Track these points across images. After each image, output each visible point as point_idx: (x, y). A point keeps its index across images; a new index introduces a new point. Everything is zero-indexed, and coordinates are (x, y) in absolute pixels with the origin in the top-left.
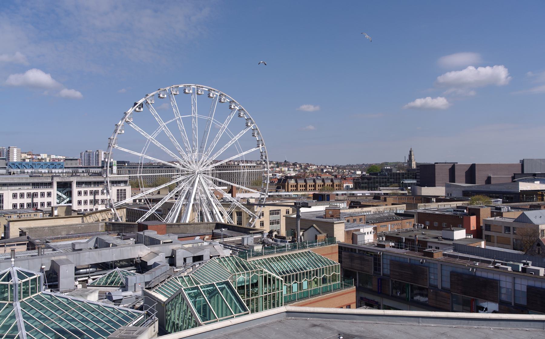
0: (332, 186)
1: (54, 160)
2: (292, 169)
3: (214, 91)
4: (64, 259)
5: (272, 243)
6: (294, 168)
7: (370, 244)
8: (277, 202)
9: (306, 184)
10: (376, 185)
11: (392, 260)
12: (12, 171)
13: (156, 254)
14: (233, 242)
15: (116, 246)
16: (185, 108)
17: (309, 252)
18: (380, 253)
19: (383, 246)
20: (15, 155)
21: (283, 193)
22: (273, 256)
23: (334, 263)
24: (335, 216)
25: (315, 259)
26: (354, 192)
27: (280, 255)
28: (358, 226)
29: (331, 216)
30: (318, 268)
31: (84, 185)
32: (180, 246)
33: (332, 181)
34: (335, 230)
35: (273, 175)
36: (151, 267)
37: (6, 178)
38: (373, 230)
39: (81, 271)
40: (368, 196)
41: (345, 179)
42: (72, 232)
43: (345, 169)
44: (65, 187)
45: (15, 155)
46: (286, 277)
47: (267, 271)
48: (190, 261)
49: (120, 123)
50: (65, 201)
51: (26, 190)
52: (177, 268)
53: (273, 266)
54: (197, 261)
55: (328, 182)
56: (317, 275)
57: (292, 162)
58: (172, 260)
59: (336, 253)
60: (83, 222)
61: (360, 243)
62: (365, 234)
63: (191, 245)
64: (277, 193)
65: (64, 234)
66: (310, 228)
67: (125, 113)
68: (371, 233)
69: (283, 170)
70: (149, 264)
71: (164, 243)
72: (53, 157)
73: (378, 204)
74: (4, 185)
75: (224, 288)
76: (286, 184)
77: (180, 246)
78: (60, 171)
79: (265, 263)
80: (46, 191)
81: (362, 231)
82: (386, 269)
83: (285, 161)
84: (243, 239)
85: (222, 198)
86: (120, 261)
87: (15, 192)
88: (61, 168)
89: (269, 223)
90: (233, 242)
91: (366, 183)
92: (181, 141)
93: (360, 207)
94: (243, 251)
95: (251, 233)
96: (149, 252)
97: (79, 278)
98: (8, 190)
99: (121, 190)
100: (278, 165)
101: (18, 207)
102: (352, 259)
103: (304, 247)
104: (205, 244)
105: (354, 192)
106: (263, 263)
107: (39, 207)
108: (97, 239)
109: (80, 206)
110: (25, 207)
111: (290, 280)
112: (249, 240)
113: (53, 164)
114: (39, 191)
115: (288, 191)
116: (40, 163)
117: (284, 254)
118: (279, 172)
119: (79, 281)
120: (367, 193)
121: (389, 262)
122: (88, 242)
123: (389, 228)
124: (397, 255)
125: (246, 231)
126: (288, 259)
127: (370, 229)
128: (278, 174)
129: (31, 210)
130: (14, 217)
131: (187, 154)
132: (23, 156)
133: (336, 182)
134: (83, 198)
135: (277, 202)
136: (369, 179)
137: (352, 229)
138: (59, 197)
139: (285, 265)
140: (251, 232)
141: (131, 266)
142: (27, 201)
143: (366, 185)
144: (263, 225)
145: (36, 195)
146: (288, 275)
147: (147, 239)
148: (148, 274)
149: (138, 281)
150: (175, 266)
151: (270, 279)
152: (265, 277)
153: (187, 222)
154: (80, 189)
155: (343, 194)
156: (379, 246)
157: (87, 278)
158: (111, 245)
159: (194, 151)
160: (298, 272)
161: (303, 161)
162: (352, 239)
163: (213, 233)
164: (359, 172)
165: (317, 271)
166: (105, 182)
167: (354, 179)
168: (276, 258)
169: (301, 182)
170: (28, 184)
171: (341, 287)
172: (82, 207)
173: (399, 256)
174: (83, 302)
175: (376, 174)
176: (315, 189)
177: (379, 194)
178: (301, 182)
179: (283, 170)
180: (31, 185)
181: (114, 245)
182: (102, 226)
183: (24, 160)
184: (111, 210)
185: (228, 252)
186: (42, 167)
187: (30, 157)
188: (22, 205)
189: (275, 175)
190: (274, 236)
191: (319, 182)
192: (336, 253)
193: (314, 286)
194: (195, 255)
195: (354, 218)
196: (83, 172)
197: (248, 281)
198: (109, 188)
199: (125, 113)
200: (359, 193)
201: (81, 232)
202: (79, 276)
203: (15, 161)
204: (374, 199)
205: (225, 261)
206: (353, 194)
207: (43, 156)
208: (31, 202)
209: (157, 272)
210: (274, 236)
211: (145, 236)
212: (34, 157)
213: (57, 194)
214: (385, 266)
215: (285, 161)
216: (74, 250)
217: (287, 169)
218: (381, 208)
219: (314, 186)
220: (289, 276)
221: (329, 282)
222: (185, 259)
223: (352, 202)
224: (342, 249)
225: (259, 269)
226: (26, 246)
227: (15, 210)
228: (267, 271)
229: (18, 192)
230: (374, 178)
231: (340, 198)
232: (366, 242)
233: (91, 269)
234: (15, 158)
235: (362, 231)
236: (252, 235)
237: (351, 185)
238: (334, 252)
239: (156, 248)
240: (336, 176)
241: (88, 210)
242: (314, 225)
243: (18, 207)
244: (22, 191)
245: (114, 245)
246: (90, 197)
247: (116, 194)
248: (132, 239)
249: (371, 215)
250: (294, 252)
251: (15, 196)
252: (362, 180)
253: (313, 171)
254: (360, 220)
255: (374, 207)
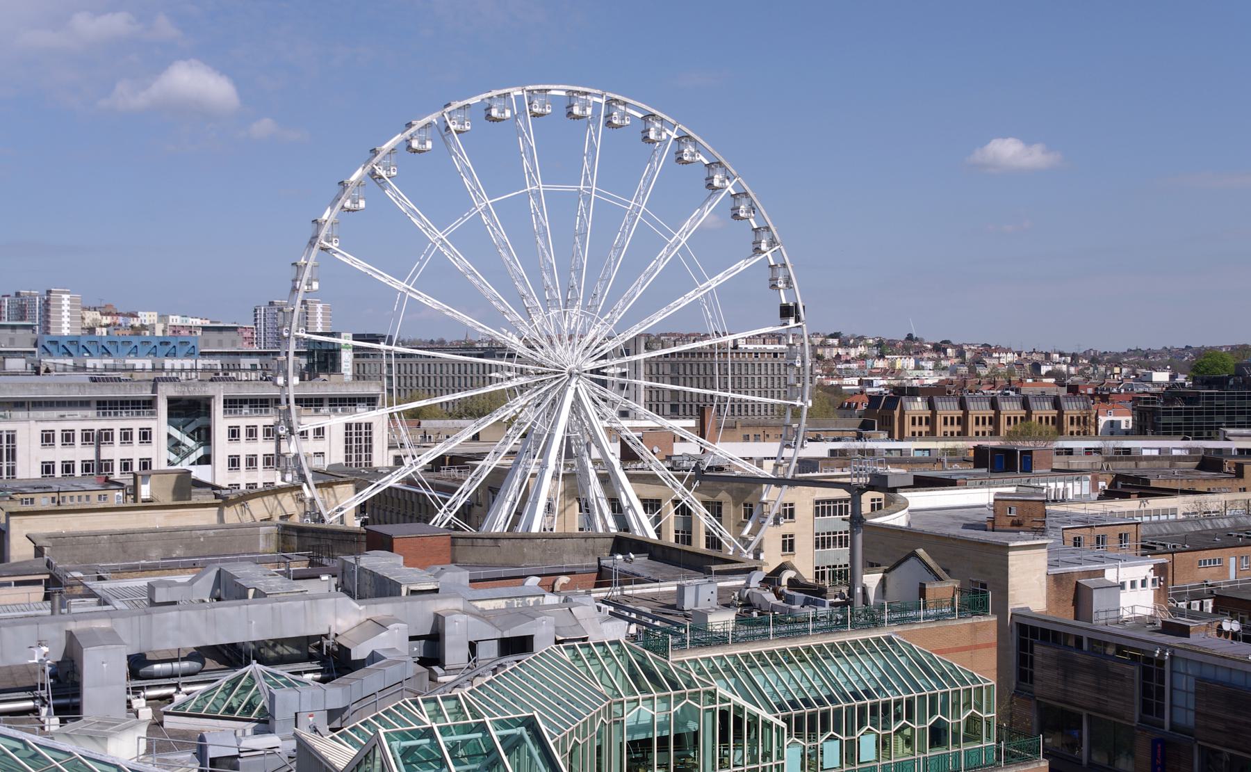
0: (1058, 421)
1: (176, 329)
2: (930, 365)
3: (625, 104)
4: (102, 630)
5: (773, 608)
6: (939, 359)
7: (1140, 622)
8: (837, 472)
9: (998, 414)
10: (1218, 418)
11: (1204, 679)
12: (48, 361)
13: (381, 626)
14: (653, 600)
15: (265, 595)
16: (501, 172)
17: (890, 640)
18: (1162, 654)
19: (1184, 631)
20: (66, 314)
21: (880, 443)
22: (763, 648)
23: (974, 680)
24: (1027, 523)
25: (911, 664)
26: (1127, 444)
27: (788, 645)
28: (1101, 560)
29: (1013, 524)
30: (915, 694)
31: (246, 409)
32: (459, 604)
33: (1056, 403)
34: (1011, 569)
35: (860, 382)
36: (361, 664)
37: (22, 385)
38: (1151, 576)
39: (157, 667)
40: (1180, 458)
41: (1105, 399)
42: (178, 552)
43: (1119, 364)
44: (191, 413)
45: (66, 314)
46: (799, 719)
47: (728, 694)
48: (488, 651)
49: (325, 217)
50: (193, 458)
51: (80, 422)
52: (446, 674)
53: (759, 681)
54: (513, 653)
55: (1045, 410)
56: (910, 717)
57: (931, 337)
58: (431, 650)
59: (988, 646)
60: (221, 519)
61: (1102, 616)
62: (1122, 586)
63: (502, 604)
64: (859, 445)
65: (155, 556)
66: (906, 559)
67: (341, 183)
68: (1144, 583)
69: (899, 365)
70: (356, 655)
71: (413, 592)
72: (175, 320)
73: (1212, 485)
74: (19, 404)
75: (520, 739)
76: (897, 413)
77: (459, 604)
78: (188, 363)
79: (739, 670)
80: (136, 424)
81: (1110, 575)
82: (1181, 708)
83: (910, 337)
84: (681, 589)
85: (669, 458)
86: (277, 642)
87: (48, 426)
88: (189, 355)
89: (811, 543)
90: (652, 599)
91: (1178, 413)
92: (535, 272)
93: (1140, 495)
94: (664, 627)
95: (710, 572)
96: (363, 618)
97: (149, 687)
98: (27, 420)
99: (359, 426)
100: (883, 348)
101: (58, 473)
102: (1067, 668)
103: (875, 623)
104: (551, 599)
105: (1127, 444)
106: (727, 669)
107: (117, 475)
108: (219, 573)
109: (234, 473)
110: (78, 472)
111: (812, 729)
112: (701, 593)
113: (167, 343)
114: (116, 425)
115: (901, 438)
116: (138, 341)
117: (801, 643)
118: (883, 373)
119: (148, 699)
120: (1177, 446)
121: (1192, 688)
122: (192, 582)
123: (1198, 571)
124: (1222, 663)
125: (700, 564)
126: (815, 659)
127: (1143, 570)
128: (879, 381)
129: (92, 483)
130: (43, 502)
131: (547, 310)
132: (91, 317)
133: (1072, 409)
134: (243, 448)
135: (837, 472)
136: (1190, 398)
137: (1076, 568)
138: (175, 445)
139: (799, 681)
140: (714, 568)
141: (311, 658)
142: (81, 453)
143: (1180, 419)
144: (791, 549)
145: (107, 439)
146: (807, 711)
147: (368, 577)
148: (338, 685)
149: (306, 707)
150: (442, 665)
151: (738, 722)
152: (724, 714)
153: (535, 529)
154: (234, 422)
155: (1088, 451)
156: (1168, 628)
157: (173, 690)
158: (251, 592)
159: (568, 303)
160: (844, 705)
161: (970, 337)
162: (1076, 602)
163: (600, 567)
164: (1161, 377)
165: (910, 703)
166: (283, 401)
167: (1135, 400)
168: (772, 654)
169: (947, 409)
170: (84, 404)
171: (999, 759)
172: (243, 478)
173: (1229, 664)
174: (70, 754)
175: (1220, 382)
176: (995, 433)
177: (1219, 451)
178: (947, 409)
179: (899, 365)
180: (94, 405)
181: (259, 594)
182: (268, 535)
183: (92, 330)
184: (300, 488)
185: (618, 630)
186: (135, 352)
187: (107, 320)
188: (68, 467)
189: (870, 383)
190: (784, 582)
191: (1011, 409)
192: (988, 646)
193: (900, 752)
194: (507, 635)
195: (1099, 531)
196: (254, 368)
197: (662, 726)
198: (294, 418)
199: (341, 183)
200: (1148, 447)
201: (206, 552)
202: (150, 682)
203: (66, 332)
204: (1199, 468)
205: (607, 654)
206: (1127, 451)
207: (147, 317)
208: (273, 451)
209: (368, 681)
210: (784, 582)
211: (362, 570)
212: (120, 320)
213: (169, 436)
214: (1180, 699)
215: (910, 337)
216: (152, 603)
217: (911, 363)
218: (1213, 502)
219: (995, 421)
220: (812, 717)
221: (956, 741)
222: (473, 646)
223: (1118, 477)
224: (1027, 637)
225: (701, 688)
226: (40, 590)
227: (46, 483)
228: (728, 694)
229: (58, 428)
230: (1210, 397)
231: (1075, 462)
232: (1126, 614)
233: (186, 665)
234: (65, 326)
235: (1110, 575)
236: (714, 578)
237: (1126, 421)
238: (980, 641)
239: (383, 609)
240: (1073, 389)
241: (243, 487)
242: (921, 551)
243: (58, 473)
244: (68, 425)
245: (259, 594)
246: (264, 447)
247: (343, 437)
248: (325, 578)
249: (1176, 521)
250: (836, 639)
251: (47, 438)
252: (1167, 401)
253: (1002, 370)
254: (1122, 538)
255: (1191, 498)
